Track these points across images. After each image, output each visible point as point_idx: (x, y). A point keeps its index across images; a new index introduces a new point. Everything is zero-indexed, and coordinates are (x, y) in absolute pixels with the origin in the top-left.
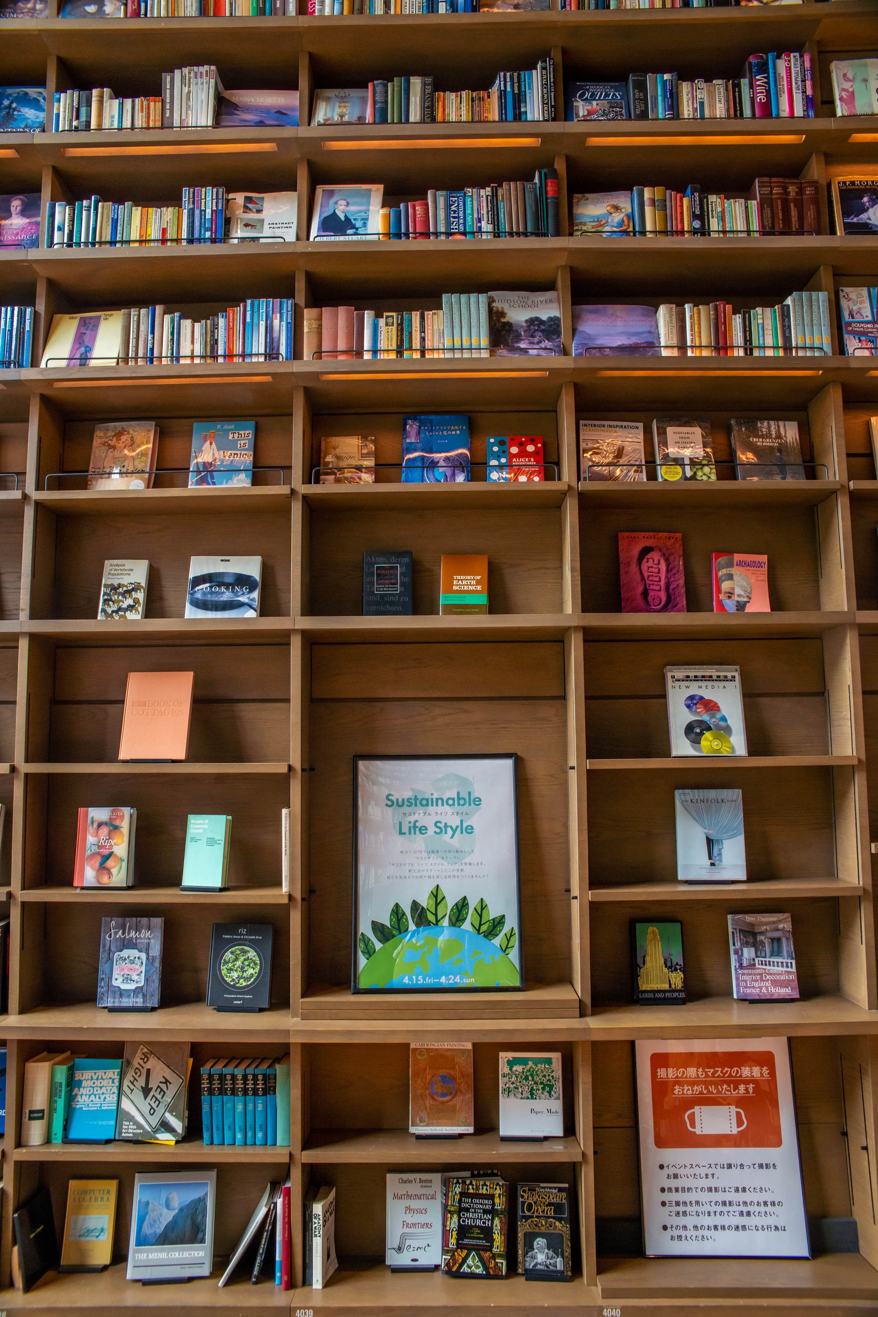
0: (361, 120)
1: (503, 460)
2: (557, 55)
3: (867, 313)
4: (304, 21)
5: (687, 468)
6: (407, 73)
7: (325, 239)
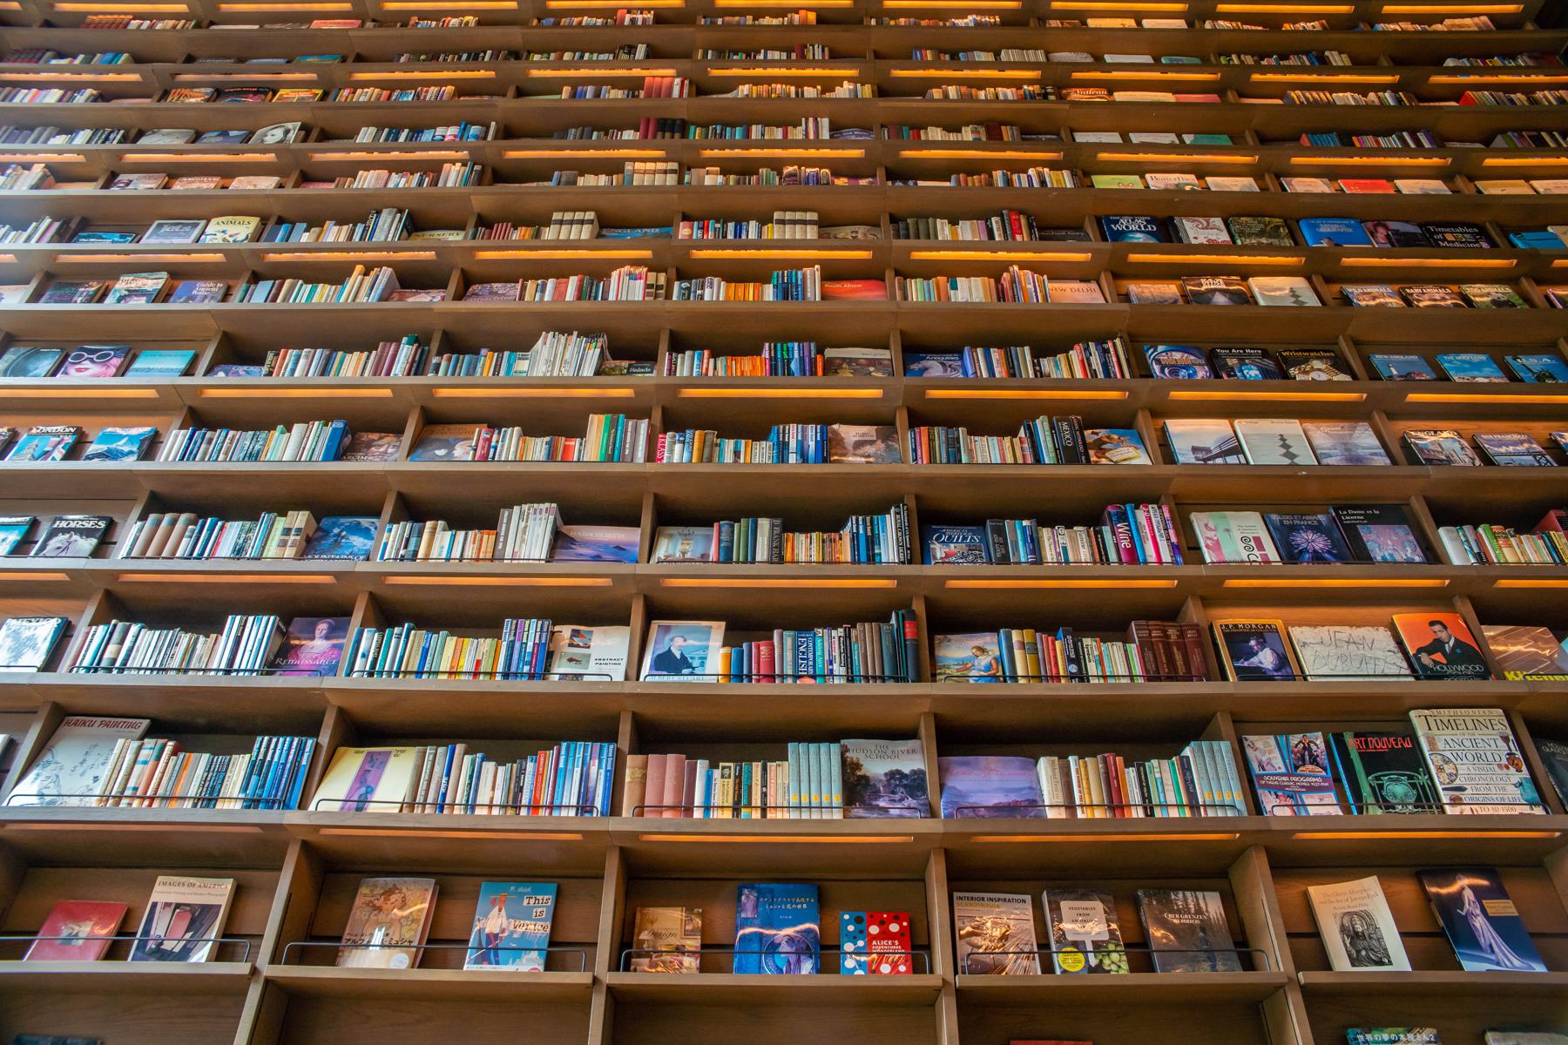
0: (704, 558)
1: (861, 943)
2: (912, 504)
3: (1278, 764)
4: (651, 468)
5: (1091, 956)
6: (754, 513)
7: (657, 679)
